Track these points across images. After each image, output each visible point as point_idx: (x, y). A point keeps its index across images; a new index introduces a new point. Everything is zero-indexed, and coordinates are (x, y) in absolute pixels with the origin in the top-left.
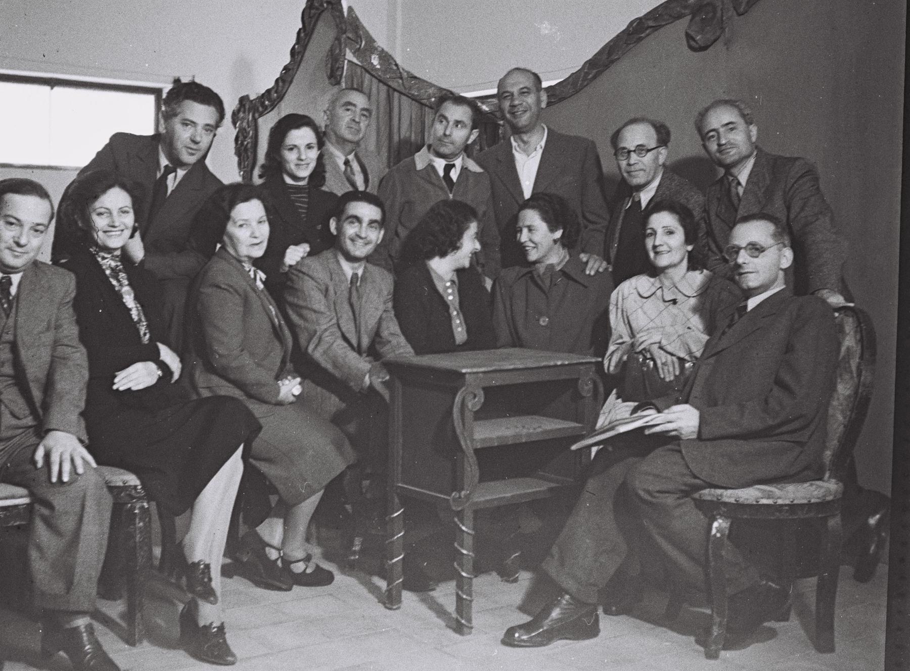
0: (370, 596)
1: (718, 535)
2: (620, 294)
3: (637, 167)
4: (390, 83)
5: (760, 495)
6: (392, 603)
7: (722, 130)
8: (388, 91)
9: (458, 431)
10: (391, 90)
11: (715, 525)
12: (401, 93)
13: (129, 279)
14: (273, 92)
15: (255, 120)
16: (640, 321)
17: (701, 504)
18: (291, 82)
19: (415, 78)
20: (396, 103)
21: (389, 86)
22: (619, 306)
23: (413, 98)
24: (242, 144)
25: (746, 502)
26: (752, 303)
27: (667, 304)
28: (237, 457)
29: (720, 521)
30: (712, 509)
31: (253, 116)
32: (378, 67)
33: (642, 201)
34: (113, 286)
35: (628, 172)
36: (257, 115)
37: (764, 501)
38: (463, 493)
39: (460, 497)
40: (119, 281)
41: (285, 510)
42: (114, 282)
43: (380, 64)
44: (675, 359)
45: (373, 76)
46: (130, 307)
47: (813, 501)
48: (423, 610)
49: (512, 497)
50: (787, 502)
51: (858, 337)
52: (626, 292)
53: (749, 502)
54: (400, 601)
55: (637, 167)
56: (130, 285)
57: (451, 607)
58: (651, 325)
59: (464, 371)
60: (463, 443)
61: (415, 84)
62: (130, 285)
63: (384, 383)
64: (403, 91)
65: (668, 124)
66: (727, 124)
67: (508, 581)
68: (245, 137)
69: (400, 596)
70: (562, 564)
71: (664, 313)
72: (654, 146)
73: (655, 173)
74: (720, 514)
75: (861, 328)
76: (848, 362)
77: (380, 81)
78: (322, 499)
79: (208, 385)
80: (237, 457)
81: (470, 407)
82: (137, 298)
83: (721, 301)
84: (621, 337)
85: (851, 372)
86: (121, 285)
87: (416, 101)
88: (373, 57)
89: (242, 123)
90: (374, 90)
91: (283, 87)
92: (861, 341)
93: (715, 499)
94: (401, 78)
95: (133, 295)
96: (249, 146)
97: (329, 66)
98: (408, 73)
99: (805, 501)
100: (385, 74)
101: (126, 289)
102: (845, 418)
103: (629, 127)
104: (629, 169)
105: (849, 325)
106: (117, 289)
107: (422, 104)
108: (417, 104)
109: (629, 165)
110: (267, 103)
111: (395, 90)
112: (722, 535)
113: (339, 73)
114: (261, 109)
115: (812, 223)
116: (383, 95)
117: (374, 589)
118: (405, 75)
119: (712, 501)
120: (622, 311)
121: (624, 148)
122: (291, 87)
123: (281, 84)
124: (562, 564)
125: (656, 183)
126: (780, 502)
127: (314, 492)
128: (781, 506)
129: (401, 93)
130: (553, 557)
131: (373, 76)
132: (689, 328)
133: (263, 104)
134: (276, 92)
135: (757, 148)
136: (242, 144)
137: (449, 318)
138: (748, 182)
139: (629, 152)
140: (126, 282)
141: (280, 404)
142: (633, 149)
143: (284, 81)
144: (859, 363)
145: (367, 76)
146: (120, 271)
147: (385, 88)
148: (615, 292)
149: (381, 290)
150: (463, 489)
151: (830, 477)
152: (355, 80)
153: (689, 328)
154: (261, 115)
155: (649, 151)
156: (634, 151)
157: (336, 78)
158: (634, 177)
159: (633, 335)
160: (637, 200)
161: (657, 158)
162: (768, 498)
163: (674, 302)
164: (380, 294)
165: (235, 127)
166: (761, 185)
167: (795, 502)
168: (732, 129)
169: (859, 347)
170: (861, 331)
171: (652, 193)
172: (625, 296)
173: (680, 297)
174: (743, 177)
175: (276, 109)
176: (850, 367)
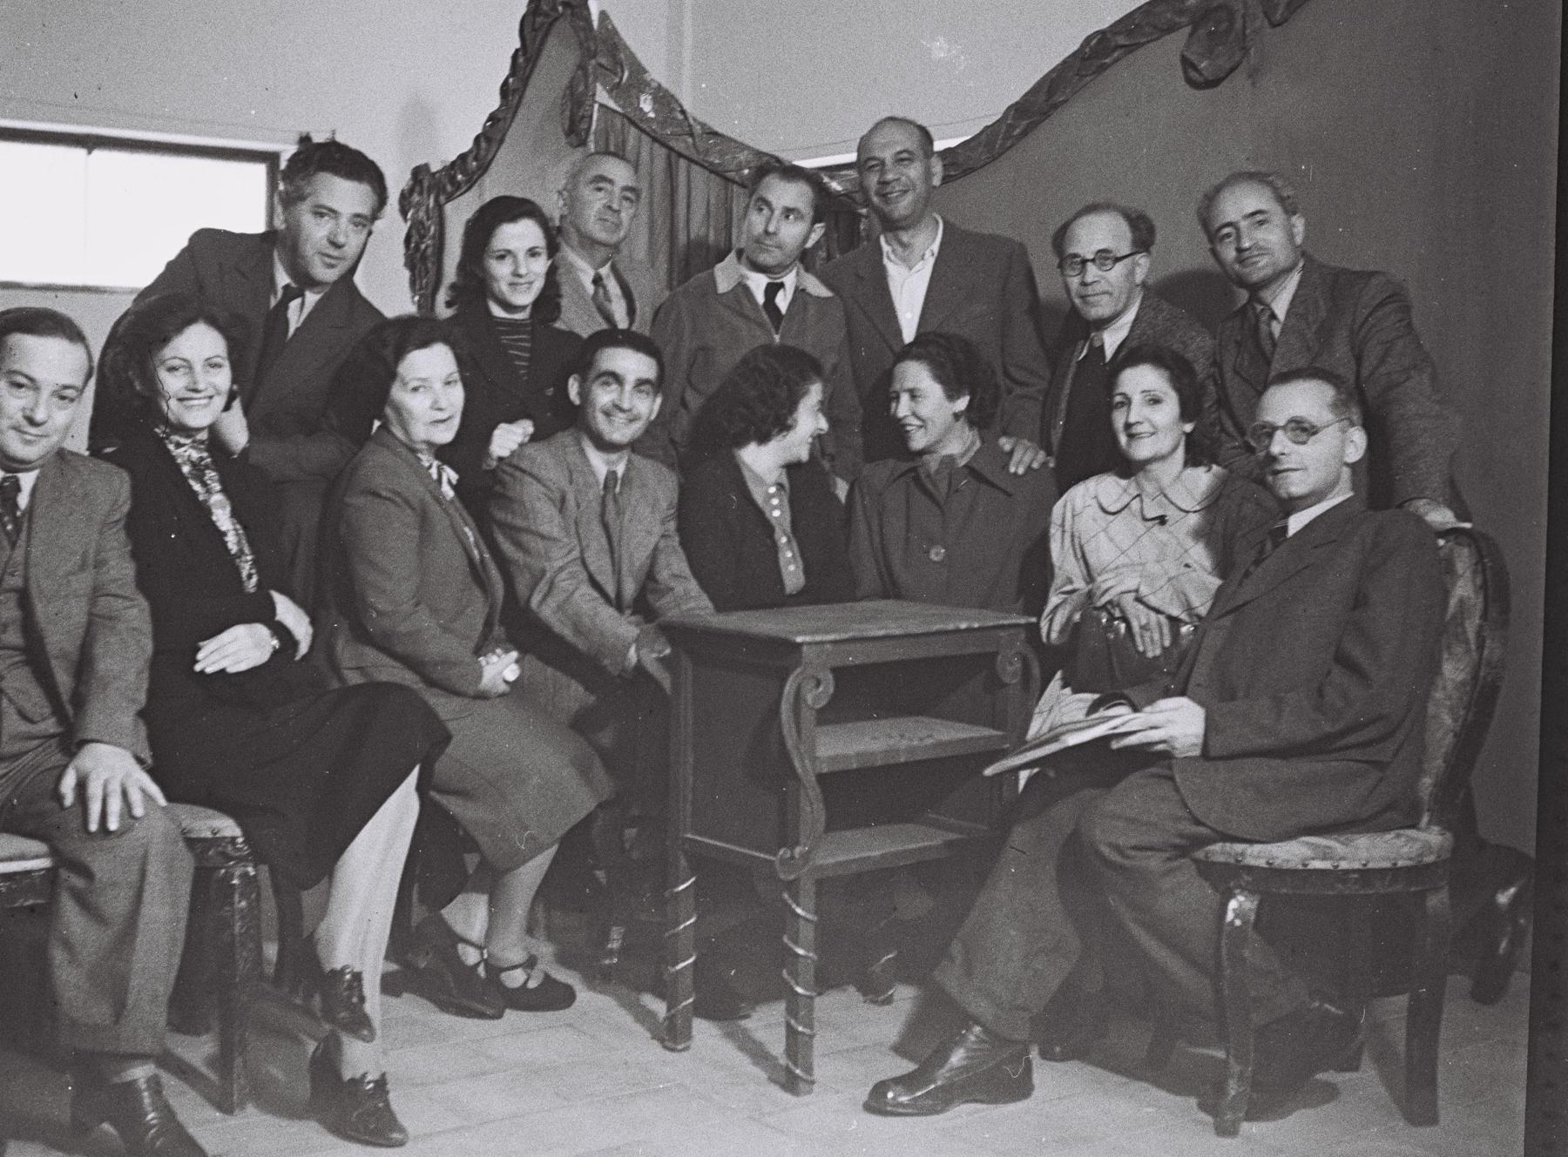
0: (638, 1028)
1: (1238, 923)
2: (1069, 507)
3: (1098, 288)
4: (672, 144)
5: (1309, 853)
6: (675, 1039)
7: (1243, 224)
8: (669, 157)
9: (790, 743)
10: (674, 155)
11: (1233, 904)
12: (691, 160)
13: (222, 481)
14: (470, 158)
15: (440, 207)
16: (1102, 553)
17: (1207, 870)
18: (501, 141)
19: (716, 134)
20: (682, 178)
21: (671, 149)
22: (1067, 527)
23: (712, 170)
24: (417, 247)
25: (1285, 866)
26: (1296, 523)
27: (1149, 524)
28: (408, 787)
29: (1241, 898)
30: (1226, 878)
31: (437, 200)
32: (652, 115)
33: (1107, 347)
34: (195, 494)
35: (1083, 297)
36: (442, 199)
37: (1317, 864)
38: (798, 850)
39: (792, 857)
40: (204, 484)
41: (491, 880)
42: (197, 487)
43: (654, 110)
44: (1162, 618)
45: (643, 131)
46: (223, 529)
47: (1400, 863)
48: (729, 1052)
49: (883, 856)
50: (1357, 866)
51: (1479, 581)
52: (1079, 504)
53: (1291, 865)
54: (689, 1037)
55: (1098, 288)
56: (224, 491)
57: (777, 1047)
58: (1122, 560)
59: (799, 639)
60: (797, 764)
61: (716, 144)
62: (224, 491)
63: (661, 660)
64: (695, 157)
65: (1151, 214)
66: (1253, 214)
67: (875, 1002)
68: (422, 237)
69: (690, 1027)
70: (969, 973)
71: (1145, 540)
72: (1126, 251)
73: (1129, 298)
74: (1240, 887)
75: (1484, 565)
76: (1462, 624)
77: (655, 140)
78: (555, 861)
79: (359, 664)
80: (408, 787)
81: (810, 701)
82: (235, 514)
83: (1243, 520)
84: (1070, 581)
85: (1467, 642)
86: (209, 492)
87: (717, 173)
88: (642, 98)
89: (417, 212)
90: (645, 155)
91: (488, 150)
92: (1484, 587)
93: (1232, 861)
94: (691, 135)
95: (228, 509)
96: (429, 251)
97: (567, 113)
98: (703, 125)
99: (1387, 865)
100: (663, 128)
101: (217, 499)
102: (1455, 721)
103: (1085, 220)
104: (1083, 291)
105: (1463, 561)
106: (201, 498)
107: (727, 180)
108: (718, 179)
109: (1084, 284)
110: (460, 177)
111: (680, 155)
112: (1245, 923)
113: (584, 126)
114: (449, 188)
115: (1398, 385)
116: (660, 164)
117: (644, 1016)
118: (698, 129)
119: (1226, 864)
120: (1072, 536)
121: (1076, 256)
122: (502, 149)
123: (483, 145)
124: (969, 973)
125: (1130, 316)
126: (1344, 865)
127: (541, 849)
128: (1346, 872)
129: (691, 160)
130: (952, 960)
131: (643, 131)
132: (1187, 566)
133: (452, 179)
134: (476, 159)
135: (1305, 255)
136: (417, 247)
137: (774, 548)
138: (1289, 313)
139: (1084, 262)
140: (217, 486)
141: (483, 696)
142: (1091, 256)
143: (489, 140)
144: (1481, 626)
145: (633, 130)
146: (207, 467)
147: (663, 151)
148: (1060, 503)
149: (656, 500)
150: (797, 843)
151: (1430, 823)
152: (612, 138)
153: (1187, 566)
154: (450, 198)
155: (1118, 260)
156: (1093, 260)
157: (578, 134)
158: (1093, 305)
159: (1090, 577)
160: (1097, 344)
161: (1131, 273)
162: (1324, 859)
163: (1162, 520)
164: (654, 506)
165: (405, 220)
166: (1311, 319)
167: (1370, 866)
168: (1261, 223)
169: (1481, 599)
170: (1484, 571)
171: (1124, 333)
172: (1078, 510)
173: (1171, 513)
174: (1281, 306)
175: (475, 187)
176: (1465, 632)
